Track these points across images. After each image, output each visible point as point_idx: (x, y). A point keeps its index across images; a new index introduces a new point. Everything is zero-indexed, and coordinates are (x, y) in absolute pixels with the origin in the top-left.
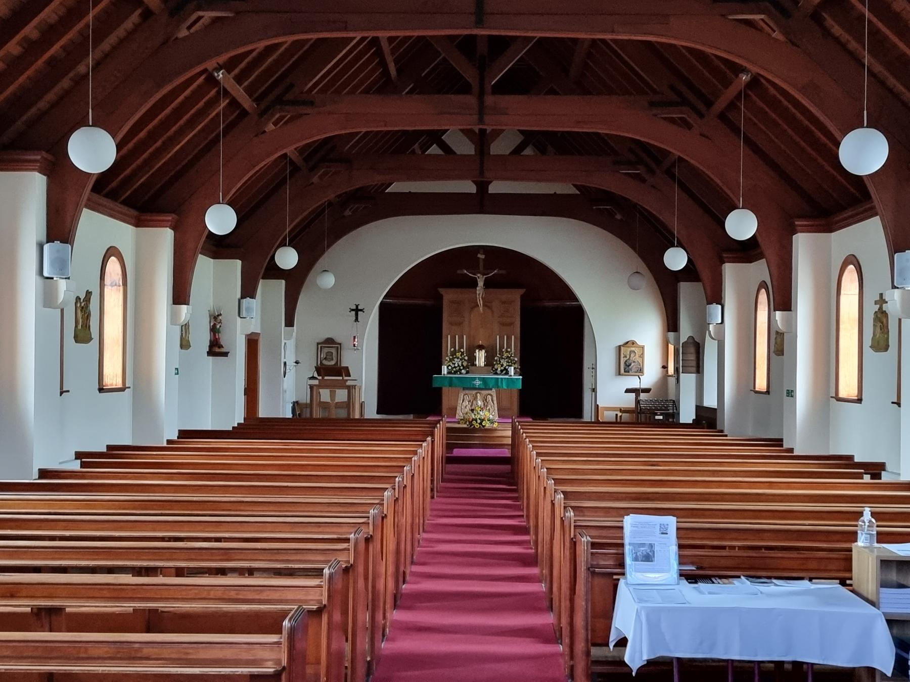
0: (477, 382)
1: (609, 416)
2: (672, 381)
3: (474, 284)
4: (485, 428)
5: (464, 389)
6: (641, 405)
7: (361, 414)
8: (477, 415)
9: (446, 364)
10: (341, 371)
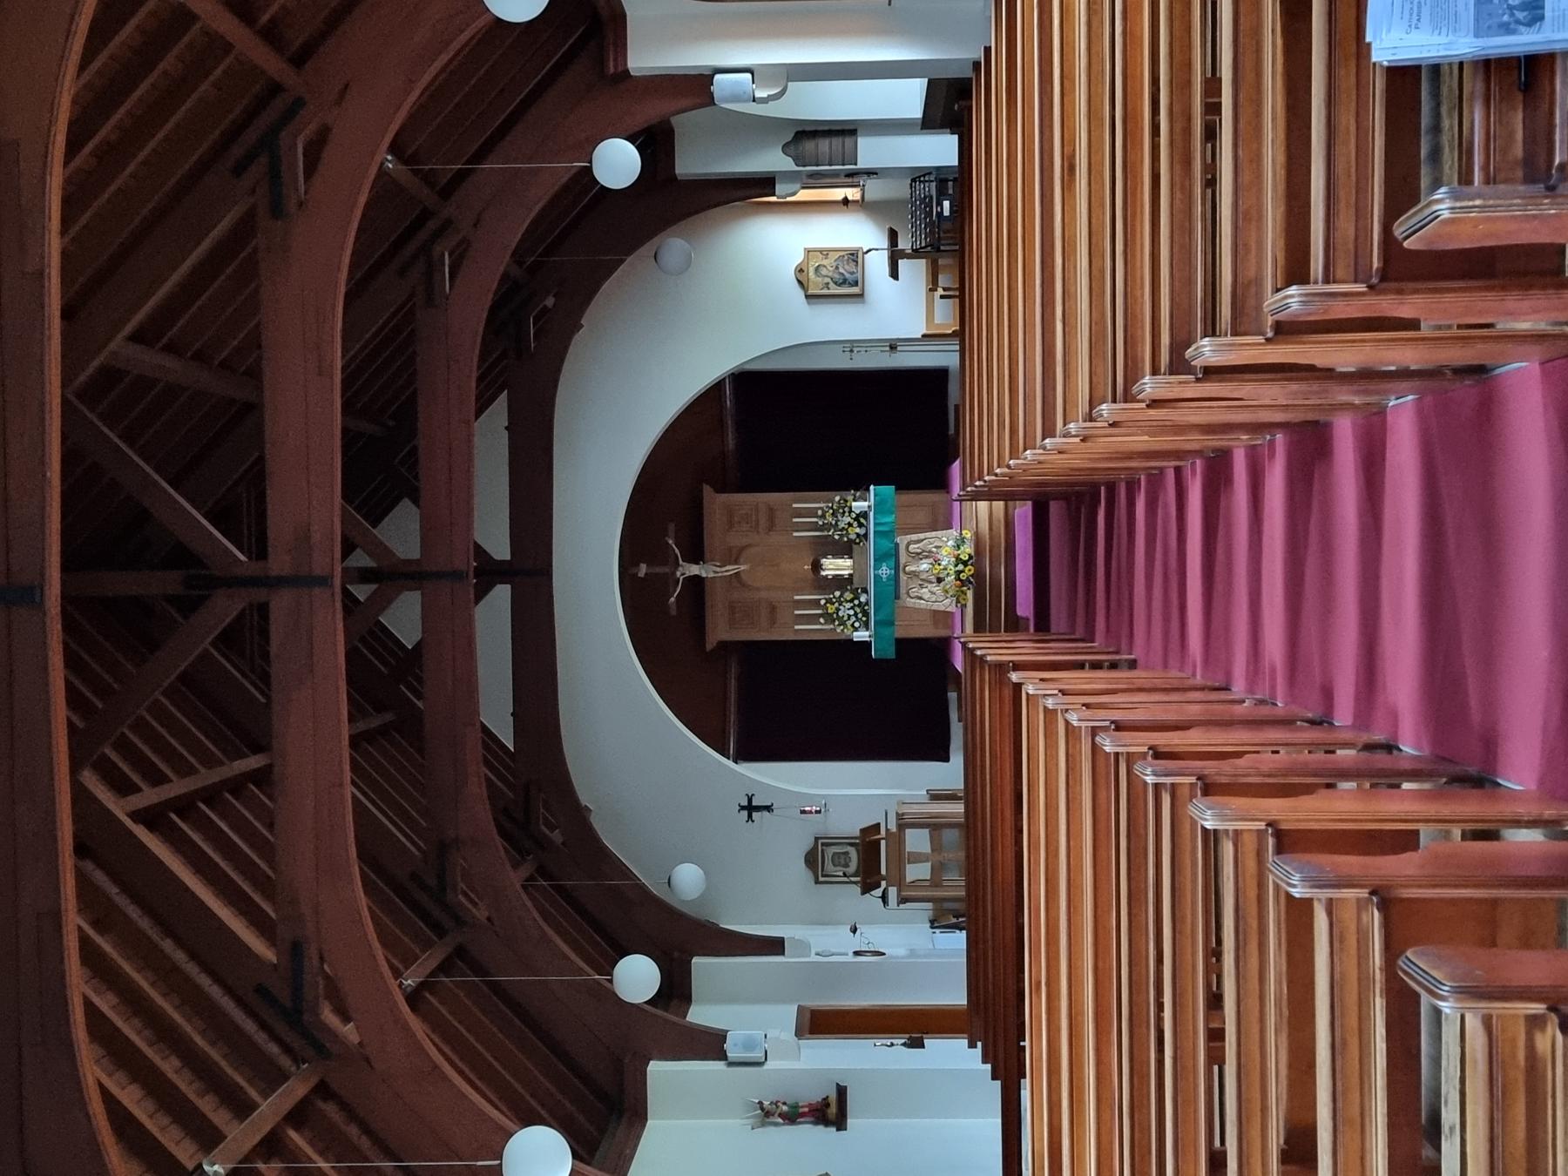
0: (884, 572)
1: (945, 316)
2: (876, 189)
3: (697, 581)
4: (973, 554)
5: (897, 597)
6: (923, 245)
7: (951, 797)
8: (948, 571)
9: (849, 633)
10: (868, 842)
